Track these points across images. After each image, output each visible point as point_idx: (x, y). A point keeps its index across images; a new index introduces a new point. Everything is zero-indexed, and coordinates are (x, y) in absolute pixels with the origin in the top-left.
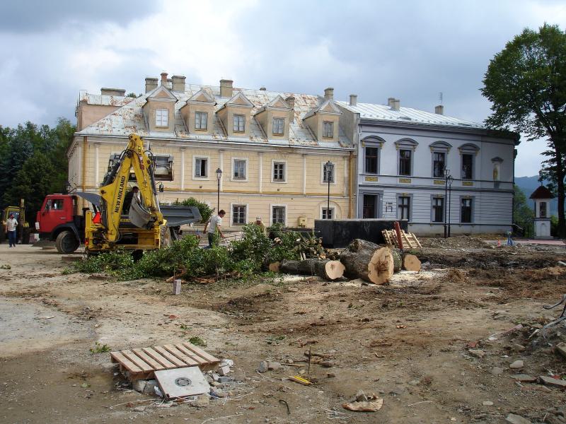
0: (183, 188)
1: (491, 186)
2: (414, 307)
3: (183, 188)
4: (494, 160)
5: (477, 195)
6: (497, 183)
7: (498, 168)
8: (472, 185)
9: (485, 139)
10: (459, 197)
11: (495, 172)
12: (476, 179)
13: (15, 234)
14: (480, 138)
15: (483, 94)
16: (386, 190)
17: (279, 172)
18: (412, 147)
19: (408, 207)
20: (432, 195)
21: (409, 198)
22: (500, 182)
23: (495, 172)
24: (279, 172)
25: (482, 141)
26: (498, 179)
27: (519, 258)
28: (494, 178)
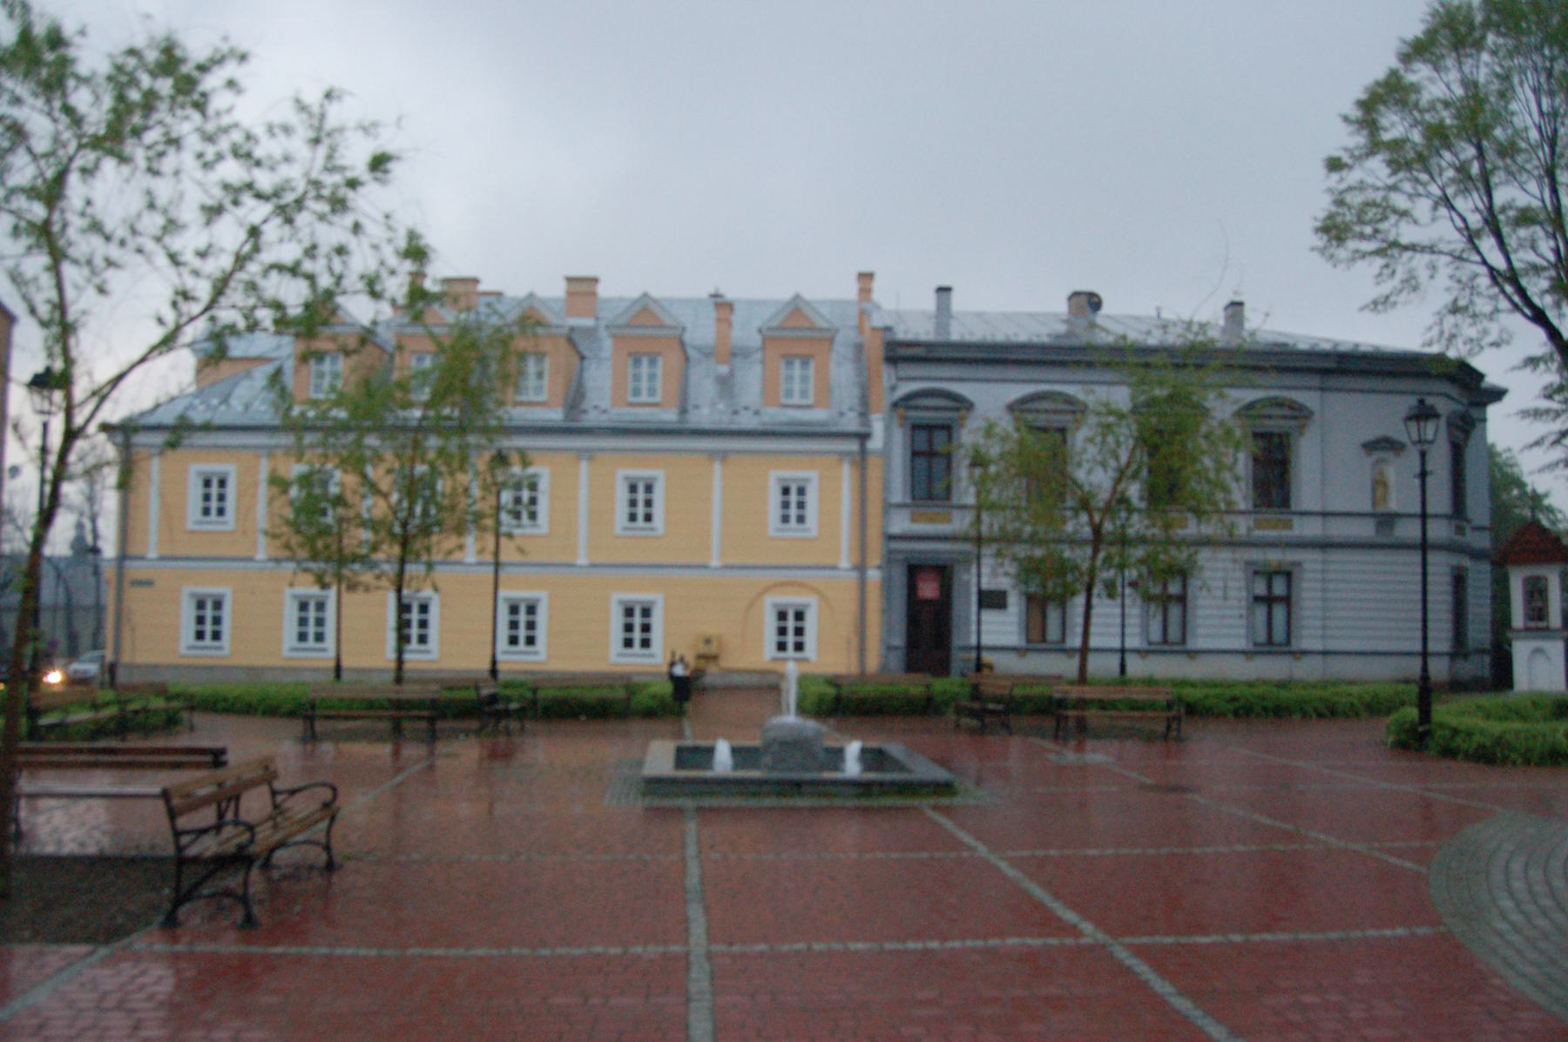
0: (715, 563)
1: (1365, 530)
2: (64, 754)
3: (715, 563)
4: (1371, 446)
5: (1310, 559)
6: (1386, 520)
7: (1391, 473)
8: (1289, 526)
9: (1332, 382)
10: (1447, 570)
11: (1379, 484)
12: (1305, 507)
13: (828, 775)
14: (1315, 381)
15: (475, 281)
16: (1204, 555)
17: (640, 500)
18: (1069, 417)
19: (1287, 600)
20: (1248, 563)
21: (1288, 575)
22: (1398, 515)
23: (1379, 484)
24: (640, 500)
25: (1323, 389)
26: (1393, 505)
27: (1180, 699)
28: (1374, 503)
